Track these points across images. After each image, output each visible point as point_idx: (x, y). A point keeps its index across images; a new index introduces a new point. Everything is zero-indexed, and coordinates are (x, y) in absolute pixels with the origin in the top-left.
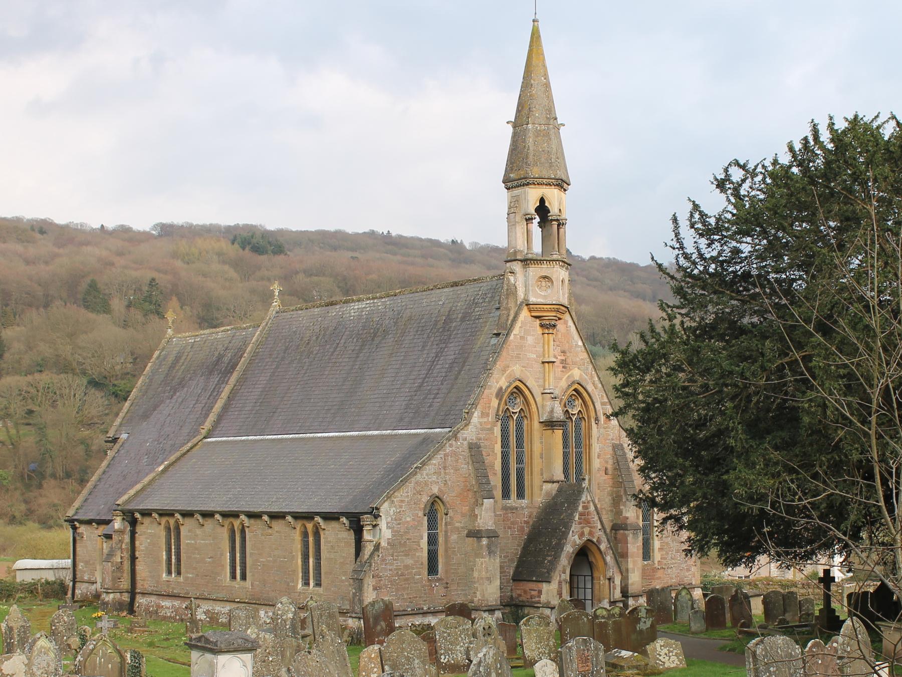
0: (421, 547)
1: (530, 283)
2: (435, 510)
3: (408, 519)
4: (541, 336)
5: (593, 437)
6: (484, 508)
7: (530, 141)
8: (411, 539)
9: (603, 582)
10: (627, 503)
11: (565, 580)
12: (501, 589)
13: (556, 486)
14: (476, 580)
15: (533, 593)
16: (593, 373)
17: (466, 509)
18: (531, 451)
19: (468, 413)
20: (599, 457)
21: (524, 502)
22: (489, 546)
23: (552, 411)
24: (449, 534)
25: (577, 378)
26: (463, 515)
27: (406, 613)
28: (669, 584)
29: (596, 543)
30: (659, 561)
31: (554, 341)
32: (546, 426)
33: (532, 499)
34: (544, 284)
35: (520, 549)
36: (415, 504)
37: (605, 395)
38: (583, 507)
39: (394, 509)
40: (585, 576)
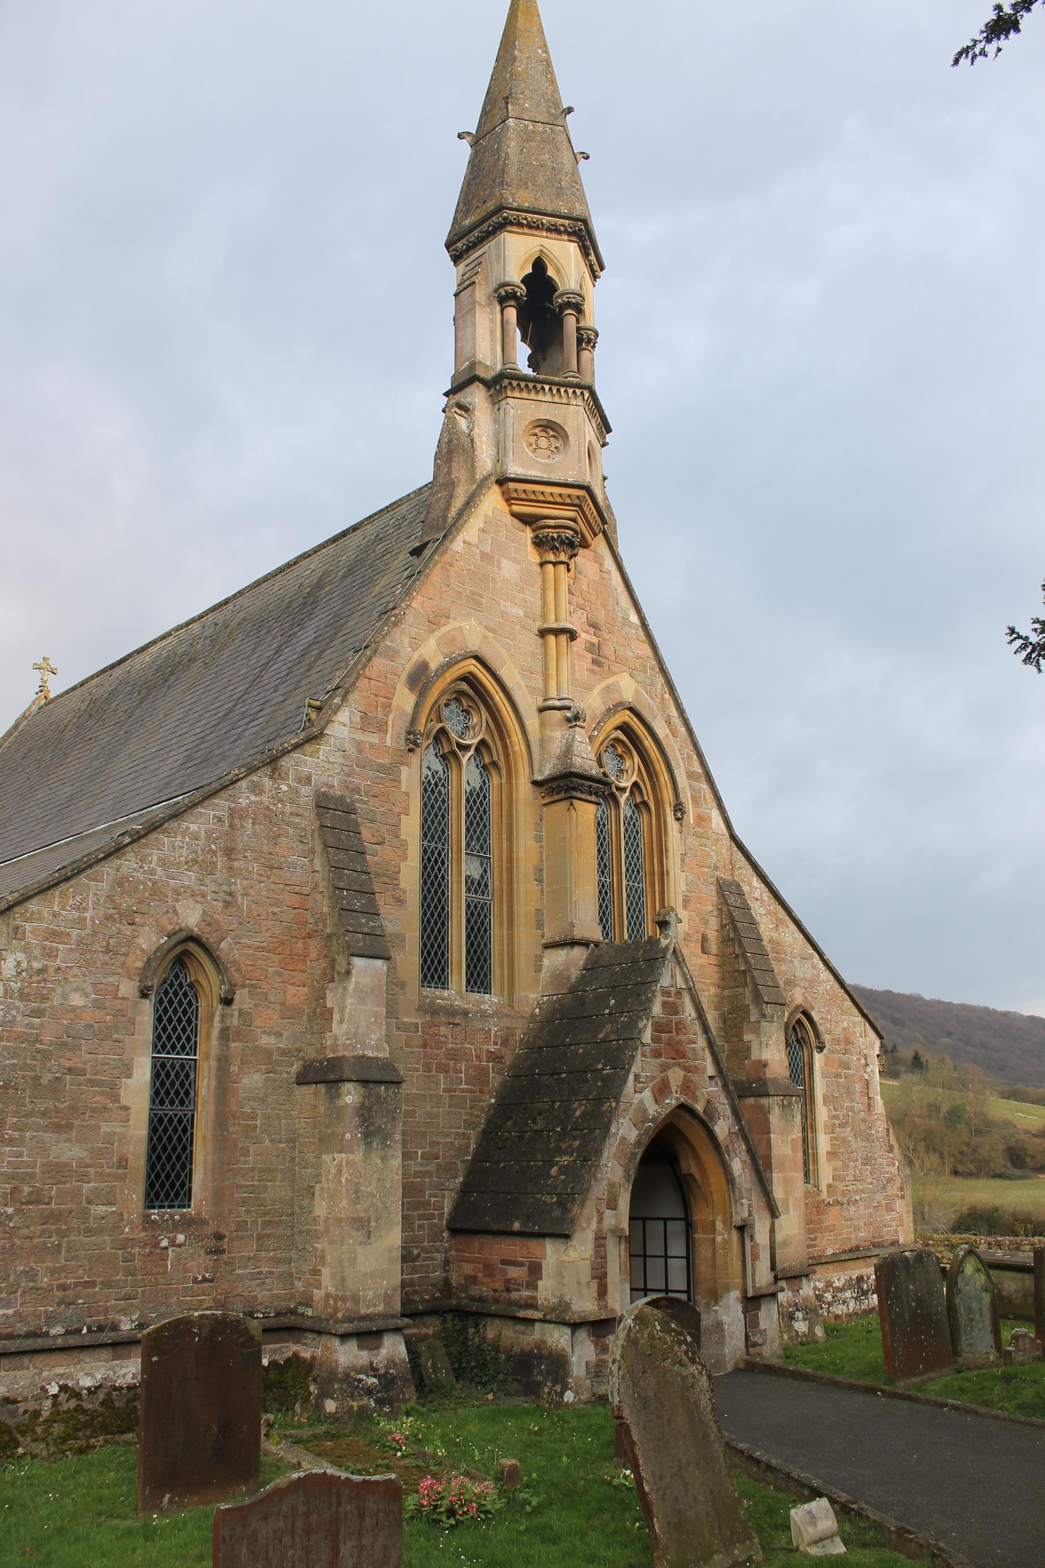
0: (124, 1101)
1: (510, 432)
2: (191, 986)
3: (77, 1000)
4: (538, 569)
5: (671, 852)
6: (351, 986)
7: (512, 146)
8: (82, 1072)
9: (723, 1235)
10: (764, 1024)
11: (616, 1231)
12: (404, 1259)
13: (579, 955)
14: (321, 1228)
15: (514, 1272)
16: (667, 696)
17: (297, 994)
18: (510, 860)
19: (319, 709)
20: (686, 902)
21: (490, 1001)
22: (365, 1114)
23: (568, 752)
24: (234, 1069)
25: (628, 697)
26: (289, 1012)
27: (40, 1343)
28: (854, 1243)
29: (705, 1118)
30: (829, 1186)
31: (570, 592)
32: (552, 792)
33: (511, 994)
34: (543, 442)
35: (473, 1135)
36: (107, 950)
37: (695, 757)
38: (664, 1004)
39: (21, 956)
40: (665, 1220)
